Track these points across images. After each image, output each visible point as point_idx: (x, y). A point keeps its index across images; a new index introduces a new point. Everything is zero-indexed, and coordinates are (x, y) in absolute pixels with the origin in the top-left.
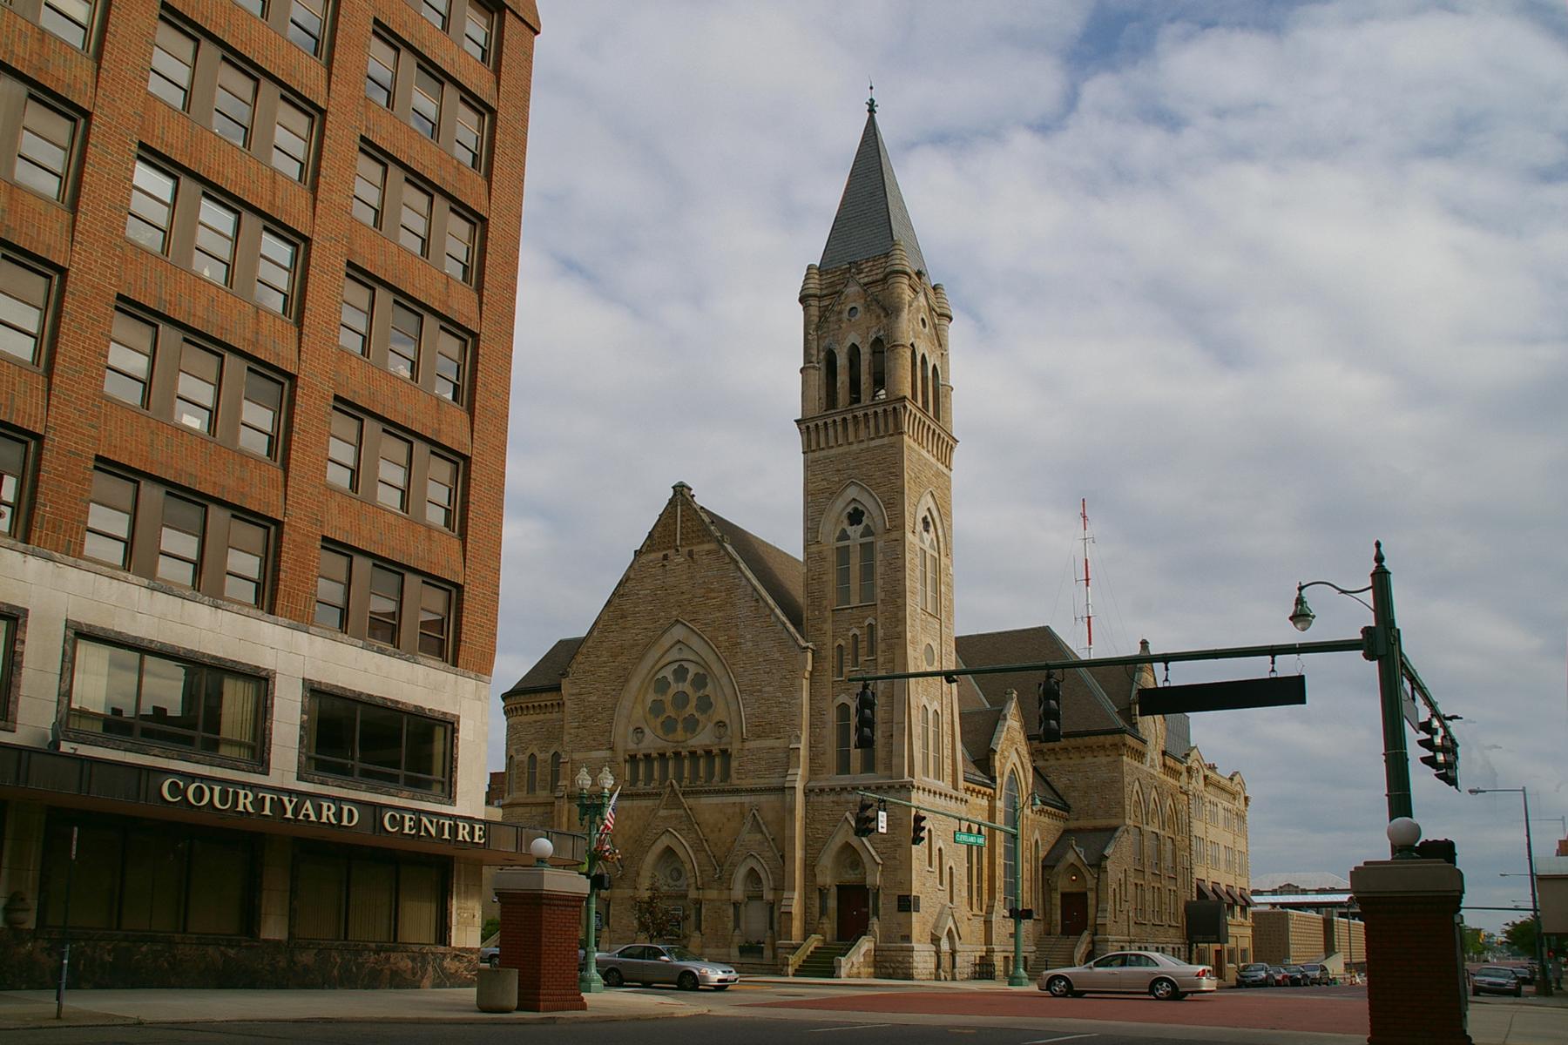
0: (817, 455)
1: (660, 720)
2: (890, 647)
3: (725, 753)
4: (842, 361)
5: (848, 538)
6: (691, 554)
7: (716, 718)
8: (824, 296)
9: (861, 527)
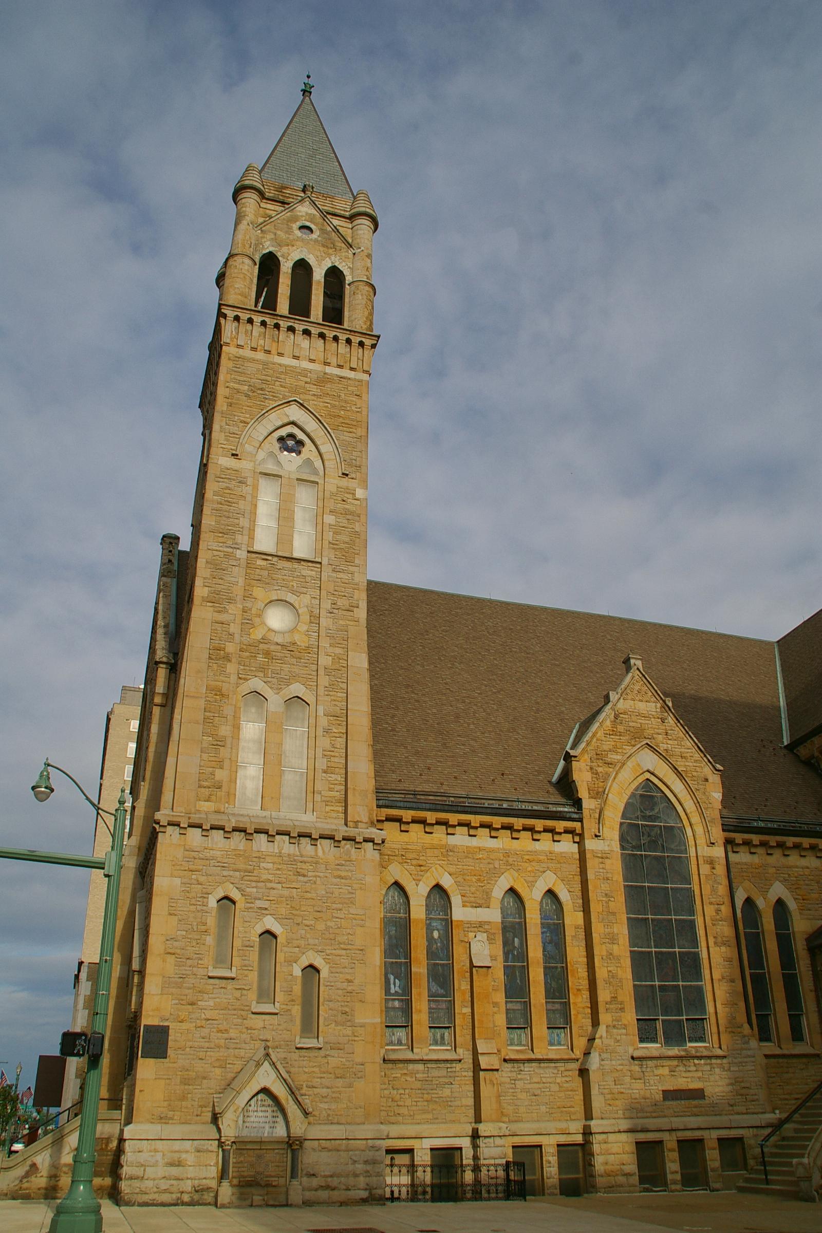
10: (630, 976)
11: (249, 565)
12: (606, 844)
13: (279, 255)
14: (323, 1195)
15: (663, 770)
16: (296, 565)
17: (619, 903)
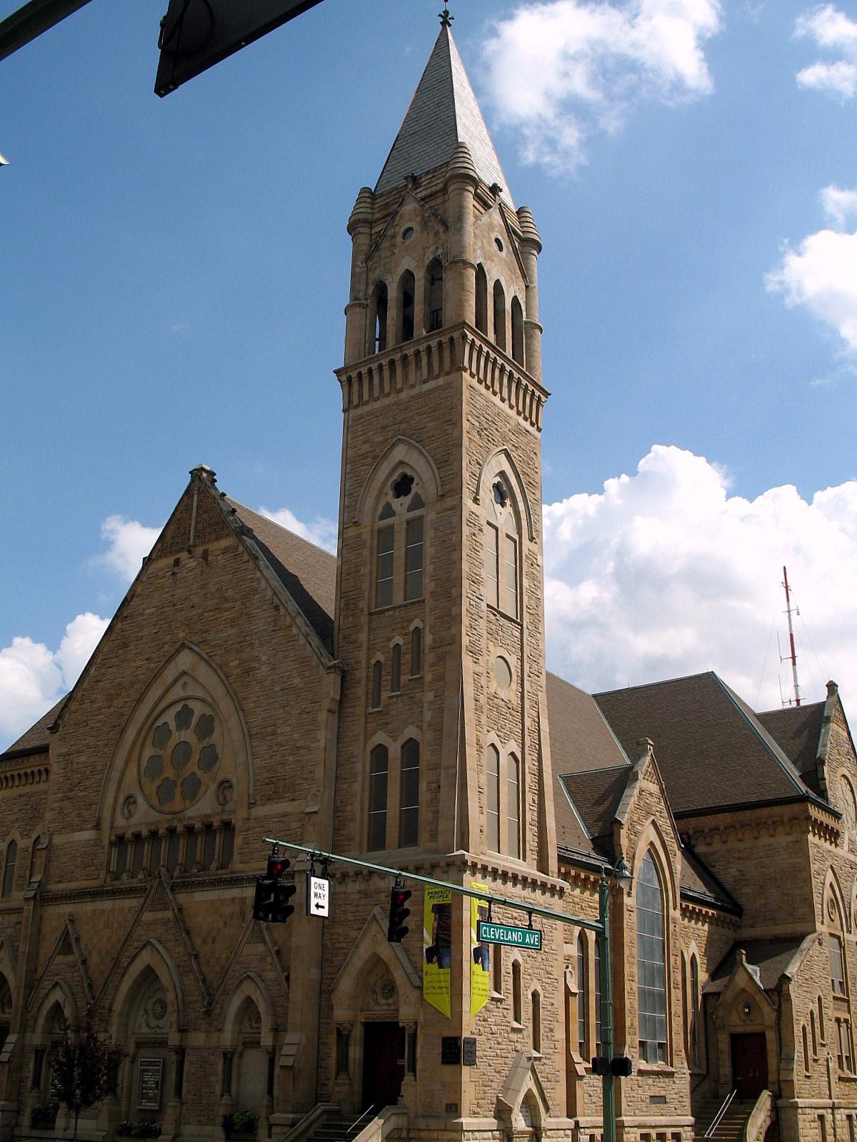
0: (359, 411)
1: (157, 782)
2: (441, 659)
3: (228, 826)
4: (393, 293)
5: (392, 514)
6: (205, 555)
7: (221, 777)
8: (374, 220)
9: (409, 497)
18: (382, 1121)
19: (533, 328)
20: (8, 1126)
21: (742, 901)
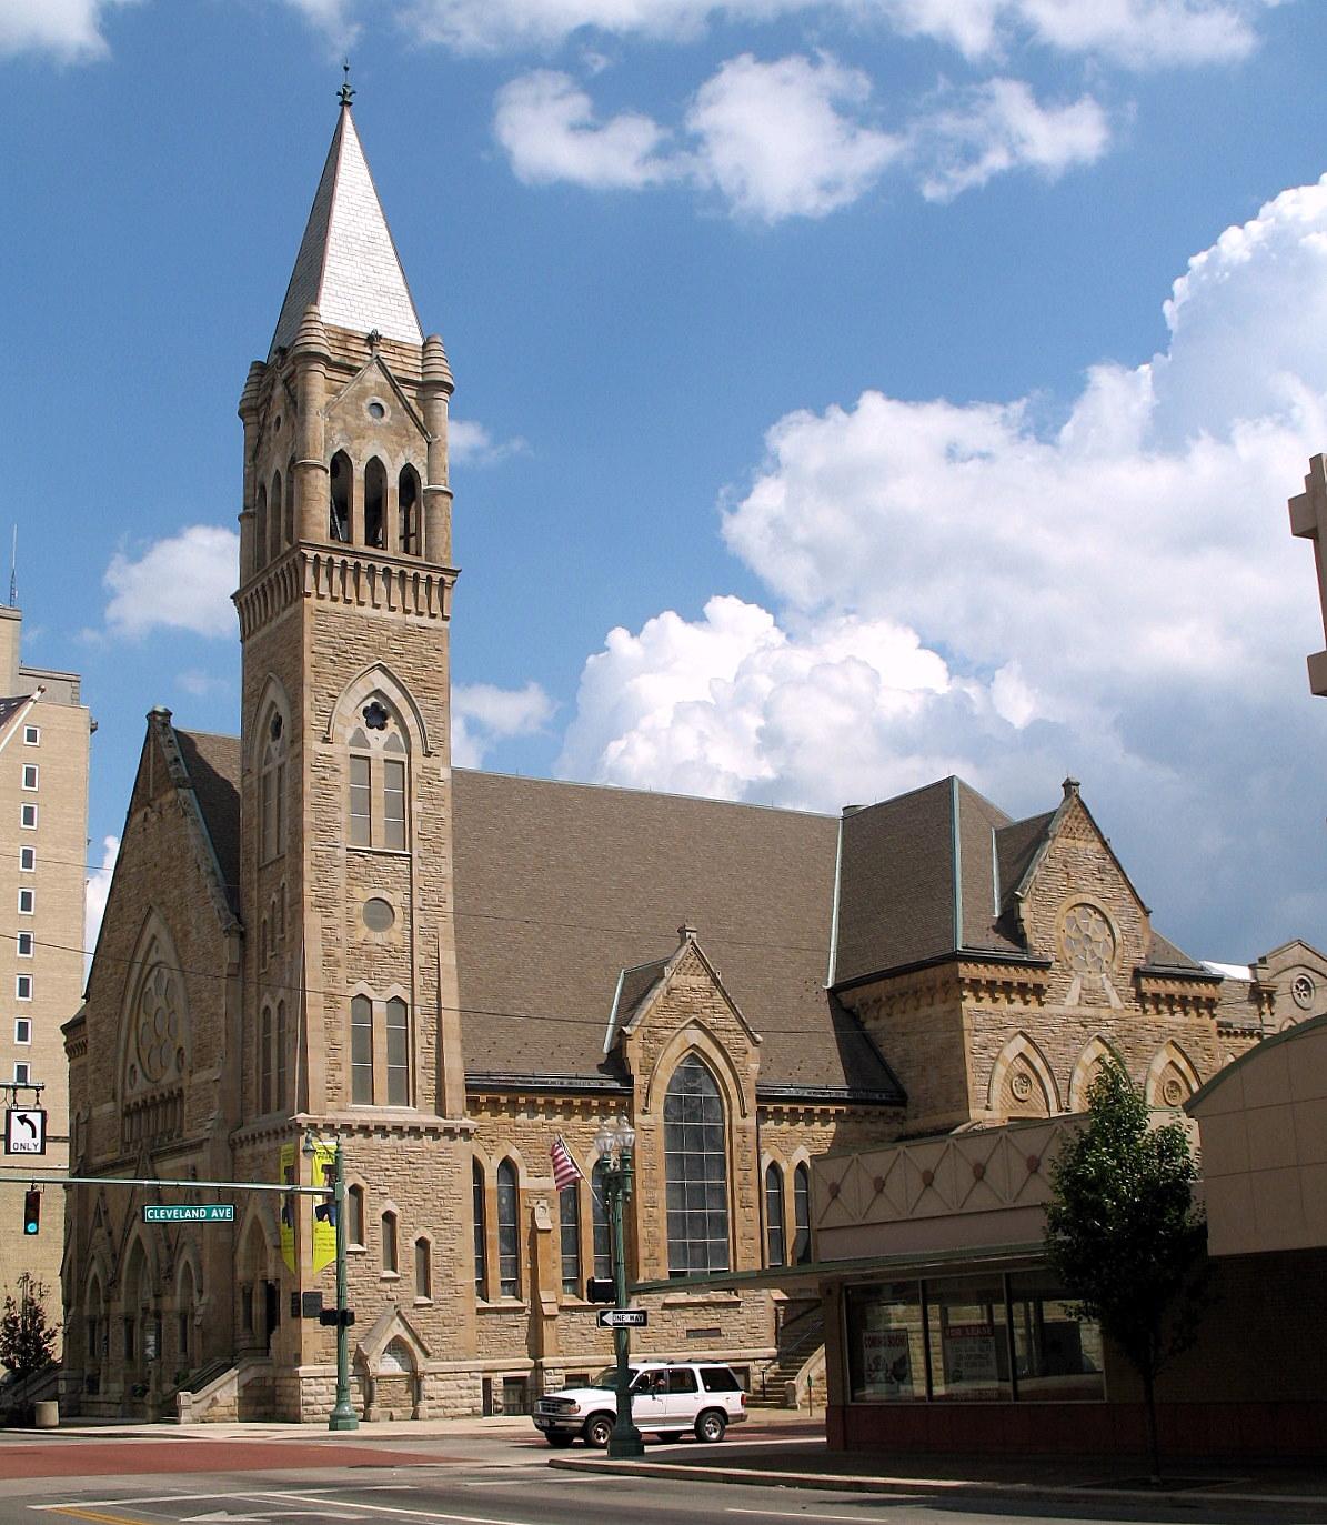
10: (666, 1235)
11: (349, 863)
12: (653, 1117)
13: (350, 453)
14: (439, 1412)
15: (707, 1045)
16: (389, 860)
17: (661, 1172)
18: (237, 1371)
19: (434, 496)
20: (74, 1392)
21: (907, 1087)
